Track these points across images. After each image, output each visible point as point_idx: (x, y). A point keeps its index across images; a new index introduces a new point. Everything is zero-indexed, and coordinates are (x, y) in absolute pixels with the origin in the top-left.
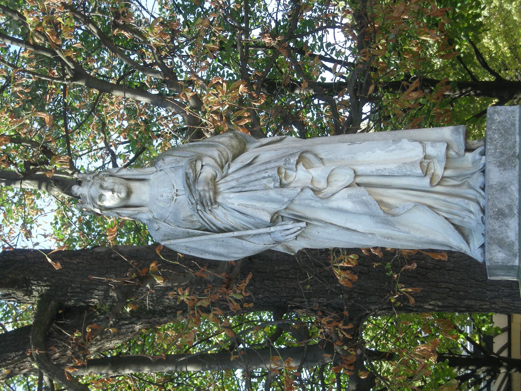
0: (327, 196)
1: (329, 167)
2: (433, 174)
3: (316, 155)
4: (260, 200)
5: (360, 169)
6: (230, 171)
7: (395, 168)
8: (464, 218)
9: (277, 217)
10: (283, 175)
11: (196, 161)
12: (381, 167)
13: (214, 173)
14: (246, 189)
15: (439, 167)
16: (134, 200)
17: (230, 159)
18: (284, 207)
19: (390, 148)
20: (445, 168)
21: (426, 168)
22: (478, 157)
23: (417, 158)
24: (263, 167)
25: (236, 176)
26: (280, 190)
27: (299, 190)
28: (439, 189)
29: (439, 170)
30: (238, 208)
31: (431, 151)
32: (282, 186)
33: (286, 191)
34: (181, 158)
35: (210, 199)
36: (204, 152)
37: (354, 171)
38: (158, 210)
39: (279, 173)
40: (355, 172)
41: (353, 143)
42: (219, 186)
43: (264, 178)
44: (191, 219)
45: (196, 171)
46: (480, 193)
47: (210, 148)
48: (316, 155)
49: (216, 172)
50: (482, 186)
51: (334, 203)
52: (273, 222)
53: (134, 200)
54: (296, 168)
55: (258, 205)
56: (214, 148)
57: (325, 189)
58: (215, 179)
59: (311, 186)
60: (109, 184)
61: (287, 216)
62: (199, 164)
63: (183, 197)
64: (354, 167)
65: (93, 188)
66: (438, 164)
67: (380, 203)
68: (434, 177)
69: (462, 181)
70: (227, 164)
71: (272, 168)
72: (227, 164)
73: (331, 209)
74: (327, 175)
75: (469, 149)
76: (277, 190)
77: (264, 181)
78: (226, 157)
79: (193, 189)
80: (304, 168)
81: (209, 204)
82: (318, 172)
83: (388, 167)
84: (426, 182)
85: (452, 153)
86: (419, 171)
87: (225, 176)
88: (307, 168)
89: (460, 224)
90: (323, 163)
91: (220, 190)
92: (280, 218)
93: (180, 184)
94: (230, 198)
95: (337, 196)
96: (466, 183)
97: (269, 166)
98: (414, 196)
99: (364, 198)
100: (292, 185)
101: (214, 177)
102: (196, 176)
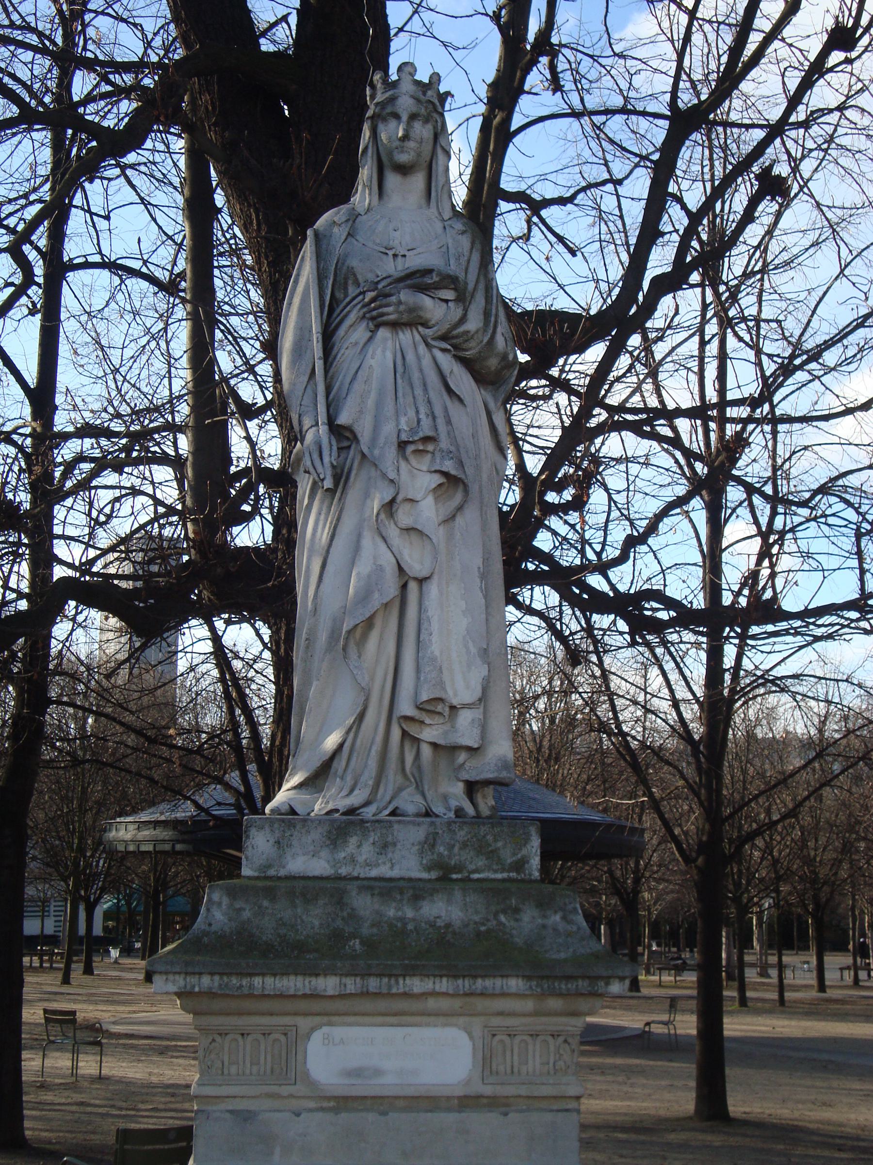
0: (382, 529)
1: (438, 535)
2: (422, 722)
3: (460, 508)
4: (379, 405)
5: (433, 589)
6: (439, 355)
7: (432, 653)
8: (342, 778)
9: (348, 439)
10: (421, 448)
11: (455, 289)
12: (435, 626)
13: (433, 322)
14: (399, 381)
15: (435, 733)
16: (392, 179)
17: (461, 354)
18: (366, 451)
19: (471, 644)
20: (435, 745)
21: (433, 708)
22: (454, 803)
23: (450, 693)
24: (438, 411)
25: (427, 361)
26: (395, 440)
27: (392, 475)
28: (396, 734)
29: (429, 734)
30: (365, 366)
31: (465, 718)
32: (402, 445)
33: (392, 452)
34: (464, 263)
35: (382, 315)
36: (473, 307)
37: (428, 578)
38: (370, 223)
39: (426, 439)
40: (426, 579)
41: (483, 576)
42: (408, 333)
43: (417, 412)
44: (350, 282)
45: (436, 289)
46: (385, 808)
47: (482, 317)
48: (460, 508)
49: (434, 326)
50: (398, 811)
51: (368, 541)
52: (336, 430)
53: (392, 179)
54: (436, 471)
55: (371, 403)
56: (481, 325)
57: (396, 524)
58: (422, 325)
59: (400, 498)
60: (418, 132)
61: (350, 456)
62: (449, 295)
63: (391, 268)
64: (435, 577)
65: (411, 101)
66: (441, 731)
67: (369, 623)
68: (417, 725)
69: (410, 776)
70: (449, 347)
71: (436, 429)
72: (449, 347)
73: (359, 537)
74: (419, 527)
75: (472, 788)
76: (395, 436)
77: (412, 413)
78: (464, 346)
79: (402, 285)
80: (434, 486)
81: (374, 313)
82: (428, 511)
83: (435, 638)
84: (406, 708)
85: (462, 757)
86: (424, 697)
87: (427, 344)
88: (435, 490)
89: (333, 770)
90: (445, 521)
91: (400, 333)
92: (345, 444)
93: (415, 262)
94: (384, 352)
95: (383, 547)
96: (408, 783)
97: (441, 421)
98: (383, 686)
99: (376, 595)
100: (403, 464)
101: (425, 325)
102: (426, 289)
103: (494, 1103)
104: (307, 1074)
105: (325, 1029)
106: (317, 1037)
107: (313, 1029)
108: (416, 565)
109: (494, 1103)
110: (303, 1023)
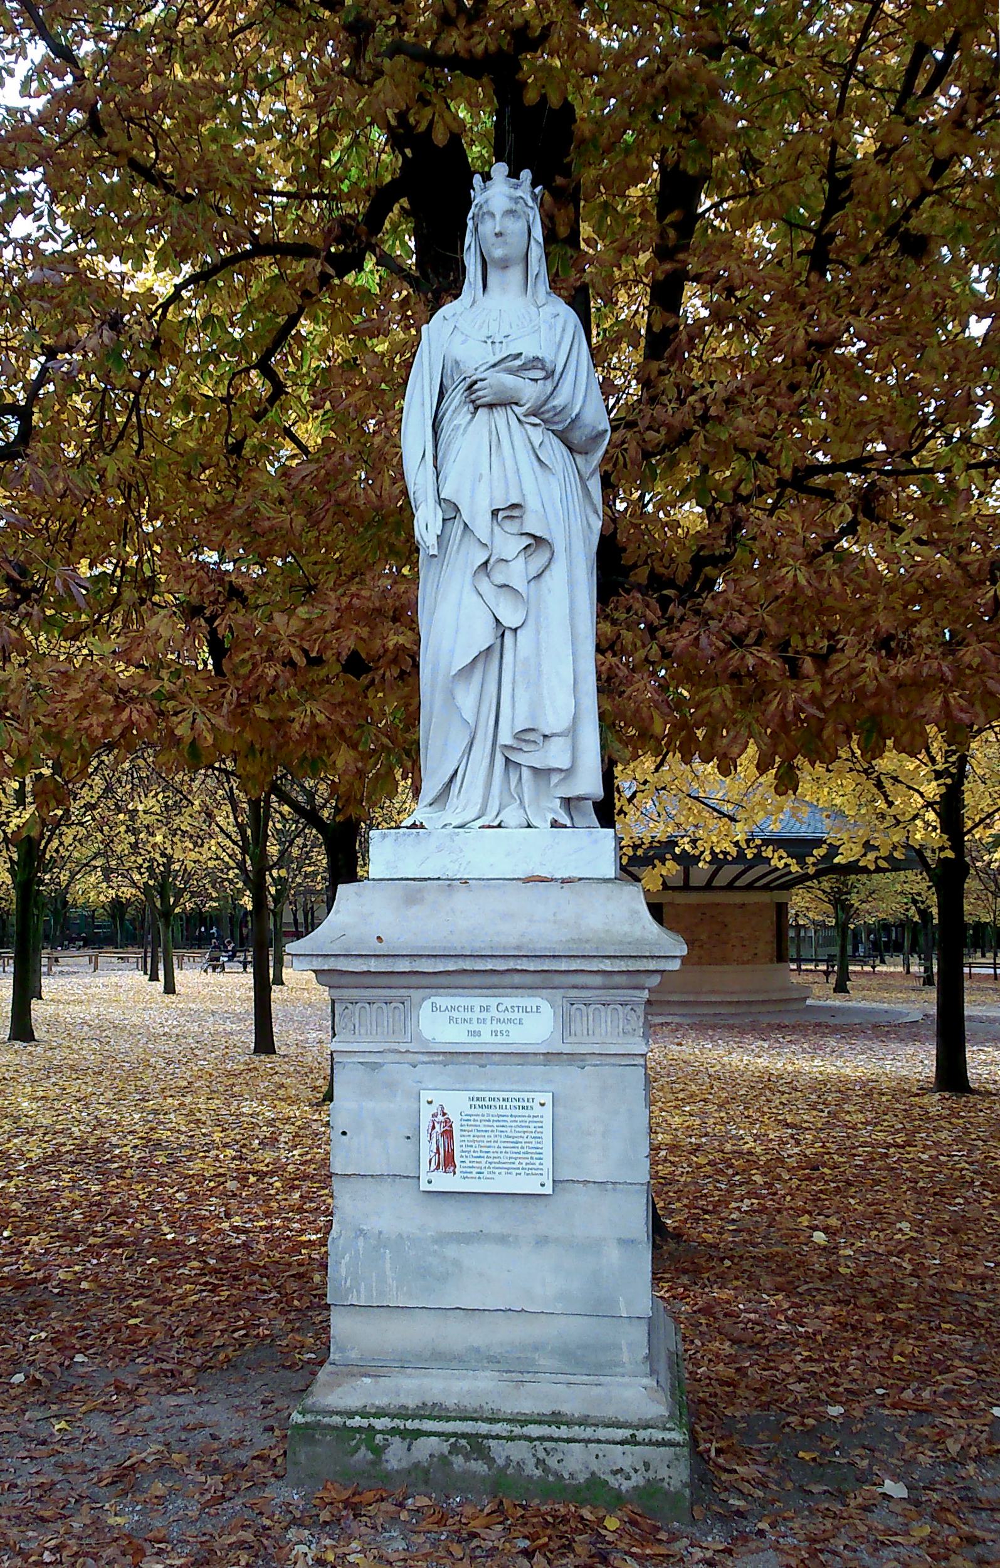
20: (533, 769)
103: (573, 1058)
104: (419, 1033)
105: (433, 999)
106: (427, 1004)
107: (424, 999)
108: (510, 619)
109: (573, 1058)
110: (416, 994)
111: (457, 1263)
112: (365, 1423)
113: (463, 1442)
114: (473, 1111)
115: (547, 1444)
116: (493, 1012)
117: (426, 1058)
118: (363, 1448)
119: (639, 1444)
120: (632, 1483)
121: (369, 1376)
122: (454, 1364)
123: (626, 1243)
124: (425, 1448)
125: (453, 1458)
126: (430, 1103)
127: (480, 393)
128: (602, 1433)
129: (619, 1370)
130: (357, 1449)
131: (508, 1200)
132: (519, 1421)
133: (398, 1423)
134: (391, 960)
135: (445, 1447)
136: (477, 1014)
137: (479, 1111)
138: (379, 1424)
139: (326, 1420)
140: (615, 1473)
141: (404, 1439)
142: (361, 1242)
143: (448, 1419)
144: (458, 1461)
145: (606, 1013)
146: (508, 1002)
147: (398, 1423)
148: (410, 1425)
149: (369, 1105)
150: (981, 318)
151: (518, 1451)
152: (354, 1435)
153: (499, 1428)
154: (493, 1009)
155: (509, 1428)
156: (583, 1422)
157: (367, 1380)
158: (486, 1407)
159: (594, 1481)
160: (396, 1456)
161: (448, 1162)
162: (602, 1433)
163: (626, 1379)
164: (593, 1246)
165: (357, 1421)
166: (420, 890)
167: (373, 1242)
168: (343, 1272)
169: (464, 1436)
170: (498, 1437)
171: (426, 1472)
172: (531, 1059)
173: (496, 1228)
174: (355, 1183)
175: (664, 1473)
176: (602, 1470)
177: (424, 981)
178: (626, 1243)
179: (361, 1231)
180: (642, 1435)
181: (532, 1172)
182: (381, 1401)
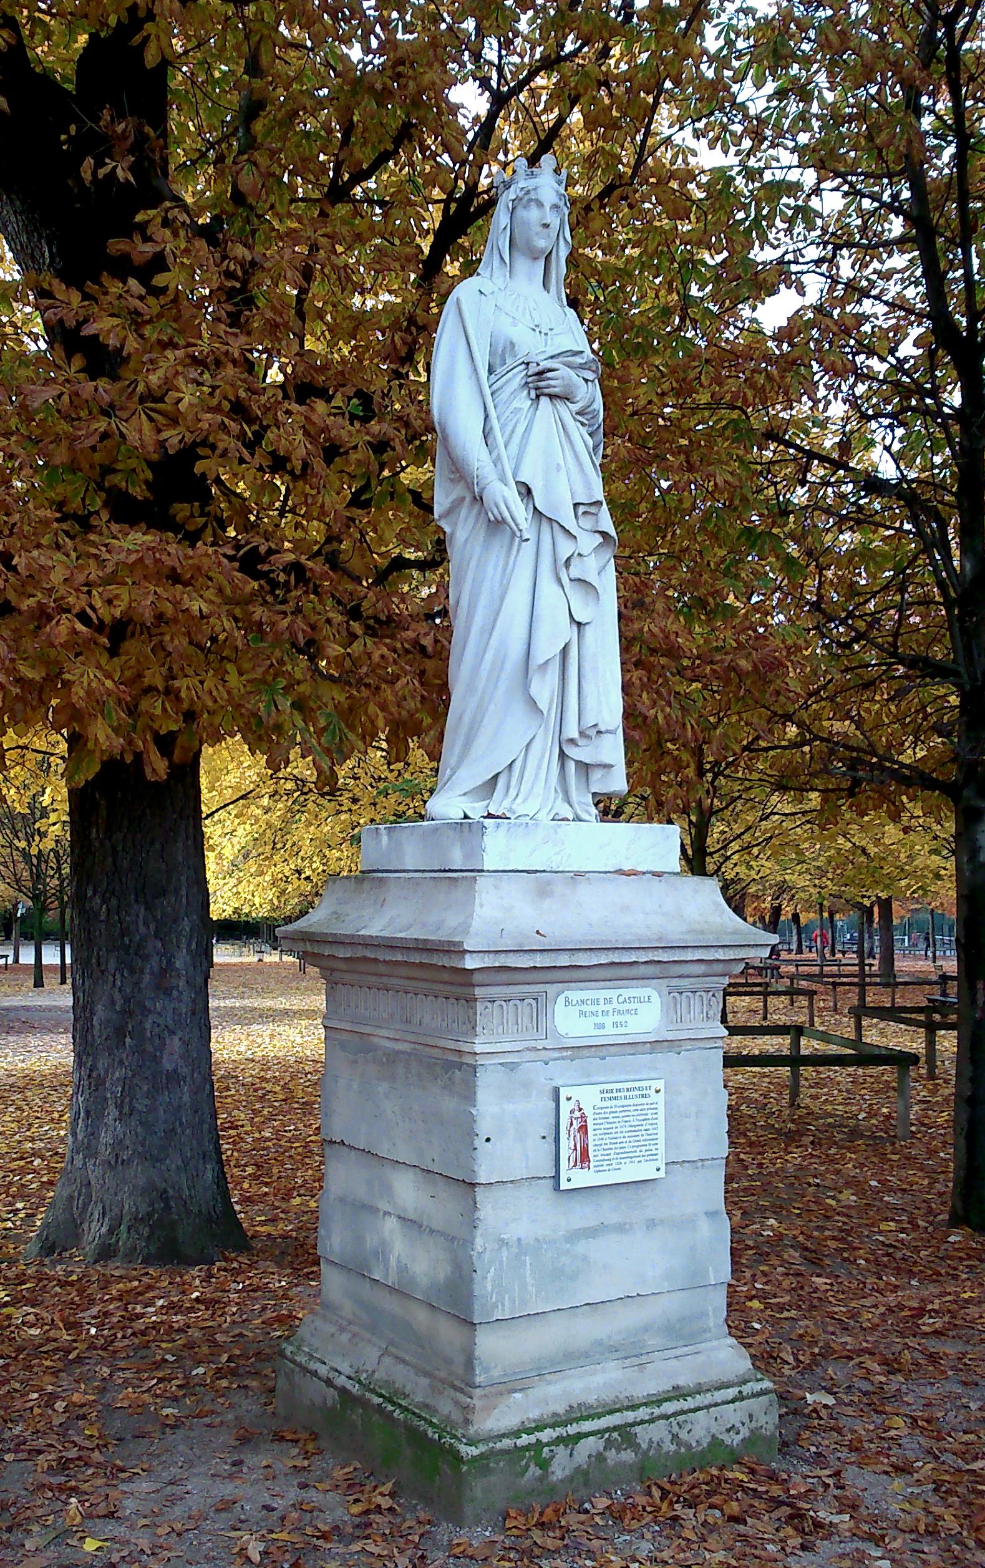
105: (566, 993)
106: (561, 999)
110: (552, 989)
111: (585, 1258)
112: (532, 1439)
113: (615, 1435)
114: (604, 1104)
115: (681, 1418)
116: (615, 1004)
117: (556, 1054)
118: (532, 1465)
119: (743, 1399)
120: (740, 1437)
121: (515, 1391)
122: (581, 1362)
123: (711, 1215)
124: (591, 1445)
125: (607, 1454)
126: (569, 1099)
127: (552, 382)
128: (719, 1396)
129: (708, 1335)
130: (527, 1466)
131: (623, 1189)
132: (653, 1402)
133: (560, 1431)
134: (553, 955)
135: (602, 1443)
136: (602, 1007)
137: (609, 1103)
138: (546, 1435)
139: (499, 1445)
140: (728, 1431)
141: (566, 1446)
142: (505, 1253)
143: (599, 1416)
144: (611, 1454)
145: (695, 1001)
146: (626, 993)
147: (560, 1431)
148: (572, 1429)
149: (510, 1107)
150: (132, 169)
151: (658, 1432)
152: (523, 1454)
153: (643, 1413)
154: (615, 1000)
155: (648, 1410)
156: (699, 1390)
157: (518, 1395)
158: (621, 1397)
159: (716, 1443)
160: (561, 1466)
161: (584, 1157)
162: (719, 1396)
163: (715, 1343)
164: (686, 1224)
165: (525, 1440)
166: (549, 883)
167: (515, 1250)
168: (489, 1288)
169: (615, 1428)
170: (642, 1422)
171: (586, 1473)
172: (640, 1048)
173: (614, 1218)
174: (498, 1193)
175: (763, 1420)
176: (717, 1429)
177: (559, 975)
178: (711, 1215)
179: (502, 1240)
180: (747, 1389)
181: (652, 1157)
182: (534, 1414)
